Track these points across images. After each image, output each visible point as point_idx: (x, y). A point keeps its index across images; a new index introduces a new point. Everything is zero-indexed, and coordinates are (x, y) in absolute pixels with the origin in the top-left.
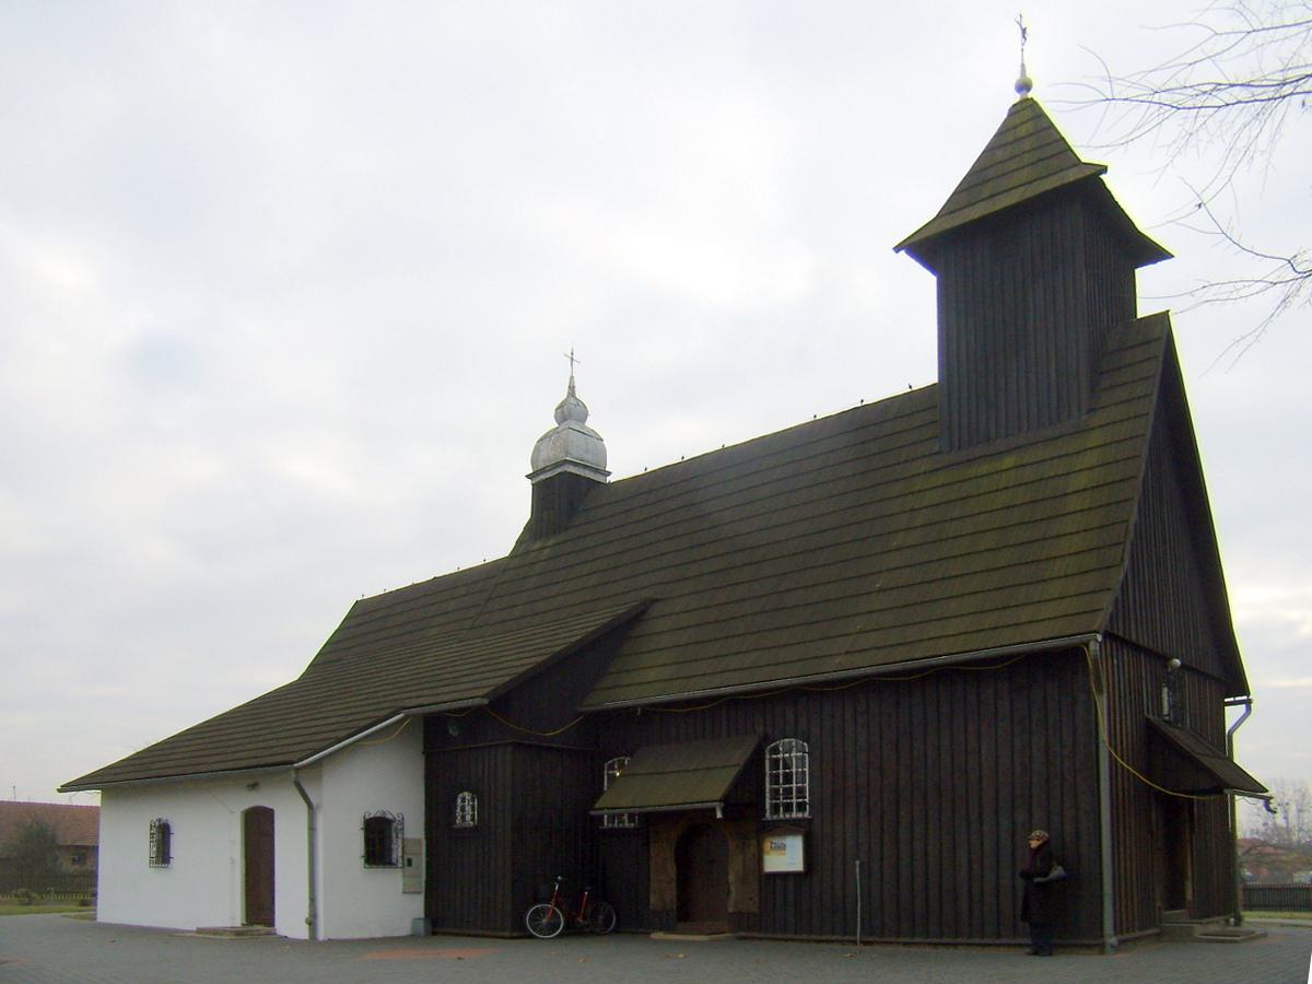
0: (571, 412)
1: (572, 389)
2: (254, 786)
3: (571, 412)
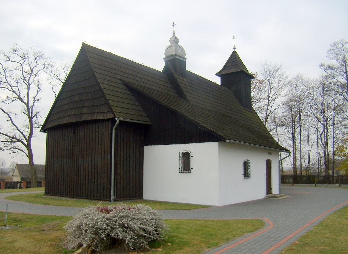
0: (175, 41)
1: (174, 33)
2: (270, 153)
3: (175, 41)
